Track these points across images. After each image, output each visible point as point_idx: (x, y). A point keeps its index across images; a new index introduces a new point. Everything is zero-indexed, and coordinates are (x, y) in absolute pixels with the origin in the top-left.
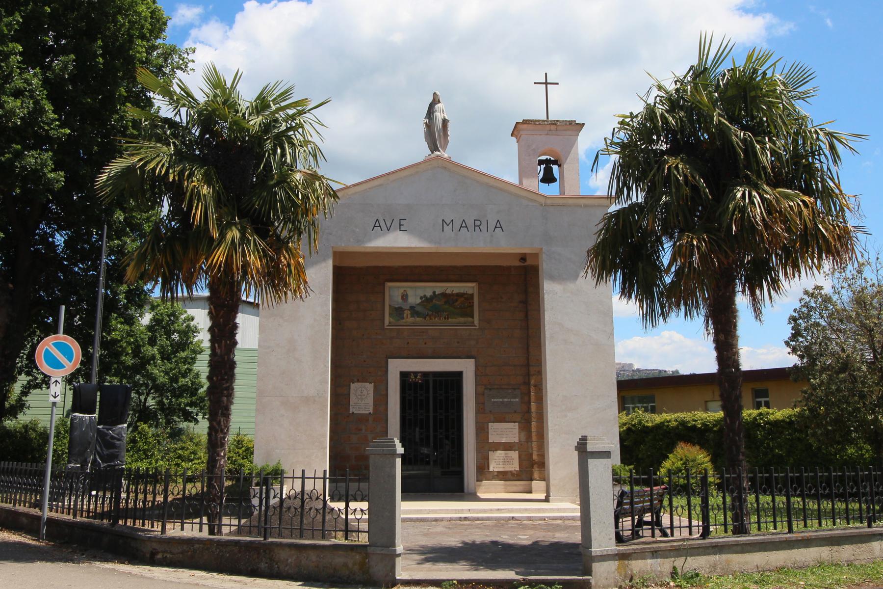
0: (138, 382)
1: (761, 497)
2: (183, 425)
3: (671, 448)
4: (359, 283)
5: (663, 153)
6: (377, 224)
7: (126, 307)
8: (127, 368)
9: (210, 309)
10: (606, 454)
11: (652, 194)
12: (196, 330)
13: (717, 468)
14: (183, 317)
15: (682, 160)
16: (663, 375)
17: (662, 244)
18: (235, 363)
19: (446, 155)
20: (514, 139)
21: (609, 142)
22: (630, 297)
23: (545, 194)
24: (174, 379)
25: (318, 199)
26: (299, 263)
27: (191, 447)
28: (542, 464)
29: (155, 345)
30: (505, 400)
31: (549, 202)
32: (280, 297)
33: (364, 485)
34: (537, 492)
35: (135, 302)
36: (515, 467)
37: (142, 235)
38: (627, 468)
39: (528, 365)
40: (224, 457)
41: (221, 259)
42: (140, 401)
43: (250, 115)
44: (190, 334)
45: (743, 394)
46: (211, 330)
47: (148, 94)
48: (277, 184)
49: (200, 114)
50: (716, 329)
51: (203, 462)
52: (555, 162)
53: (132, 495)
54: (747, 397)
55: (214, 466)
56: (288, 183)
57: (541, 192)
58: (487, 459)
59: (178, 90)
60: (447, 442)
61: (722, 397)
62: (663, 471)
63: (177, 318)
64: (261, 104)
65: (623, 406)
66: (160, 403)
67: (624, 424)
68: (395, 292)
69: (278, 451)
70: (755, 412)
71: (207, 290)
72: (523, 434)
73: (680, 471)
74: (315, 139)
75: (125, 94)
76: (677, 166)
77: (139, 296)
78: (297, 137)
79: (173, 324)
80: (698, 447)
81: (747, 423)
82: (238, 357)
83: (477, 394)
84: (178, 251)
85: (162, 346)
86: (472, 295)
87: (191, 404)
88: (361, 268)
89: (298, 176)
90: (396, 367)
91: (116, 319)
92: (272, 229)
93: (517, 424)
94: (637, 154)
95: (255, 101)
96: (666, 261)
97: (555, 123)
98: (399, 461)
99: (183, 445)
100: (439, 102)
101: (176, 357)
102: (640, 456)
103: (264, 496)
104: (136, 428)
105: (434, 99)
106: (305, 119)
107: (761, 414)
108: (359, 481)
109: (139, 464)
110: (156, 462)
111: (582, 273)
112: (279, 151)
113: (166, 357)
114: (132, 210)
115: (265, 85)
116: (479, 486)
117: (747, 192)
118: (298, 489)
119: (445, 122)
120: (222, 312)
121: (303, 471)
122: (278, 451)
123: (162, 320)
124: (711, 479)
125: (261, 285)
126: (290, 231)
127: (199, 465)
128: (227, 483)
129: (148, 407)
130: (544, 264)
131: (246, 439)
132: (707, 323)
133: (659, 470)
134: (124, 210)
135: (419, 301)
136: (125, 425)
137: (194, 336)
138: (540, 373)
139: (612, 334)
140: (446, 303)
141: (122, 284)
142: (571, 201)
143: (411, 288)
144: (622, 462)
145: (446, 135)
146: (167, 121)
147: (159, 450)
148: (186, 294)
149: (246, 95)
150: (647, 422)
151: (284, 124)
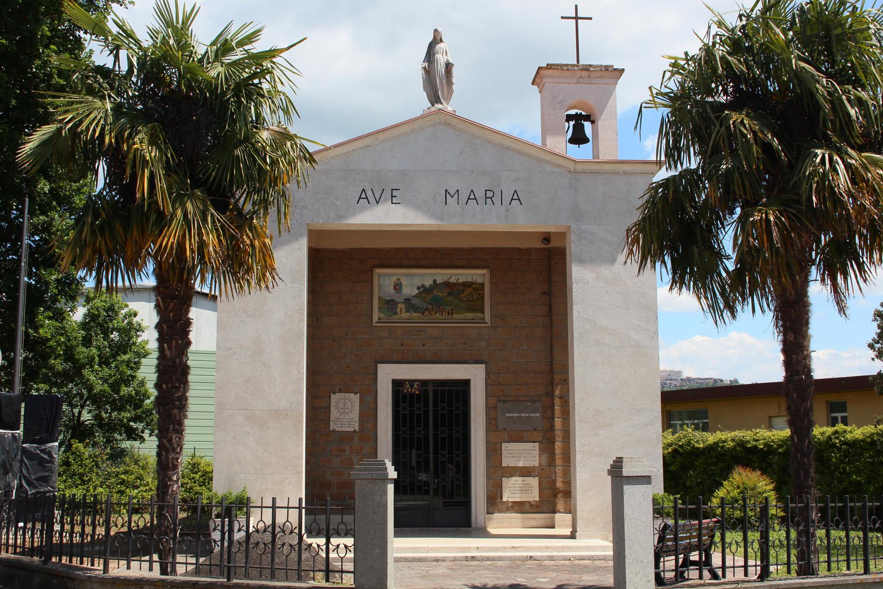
1: (833, 532)
2: (127, 444)
3: (726, 473)
4: (339, 268)
5: (722, 107)
6: (363, 196)
8: (57, 374)
10: (646, 480)
12: (139, 329)
14: (123, 312)
15: (747, 115)
16: (719, 384)
18: (188, 367)
19: (450, 109)
20: (535, 88)
26: (265, 244)
28: (568, 494)
30: (523, 415)
31: (579, 167)
32: (241, 287)
33: (348, 518)
34: (561, 526)
36: (534, 496)
37: (72, 210)
38: (672, 498)
39: (551, 372)
41: (171, 240)
42: (73, 415)
45: (814, 407)
46: (158, 326)
52: (588, 118)
53: (67, 527)
54: (819, 411)
55: (165, 493)
56: (253, 144)
59: (115, 29)
60: (450, 466)
61: (788, 408)
62: (715, 502)
63: (117, 314)
64: (223, 47)
65: (668, 422)
66: (98, 417)
67: (670, 445)
68: (386, 280)
69: (242, 476)
70: (829, 430)
72: (545, 456)
73: (737, 501)
75: (49, 34)
76: (742, 122)
79: (111, 321)
80: (759, 473)
81: (820, 443)
83: (488, 408)
84: (120, 230)
86: (483, 284)
87: (136, 419)
88: (343, 251)
89: (265, 135)
90: (388, 374)
97: (587, 68)
98: (391, 488)
100: (441, 41)
102: (688, 484)
103: (226, 528)
105: (435, 38)
110: (95, 490)
111: (622, 258)
116: (490, 519)
117: (827, 156)
119: (449, 66)
121: (274, 500)
122: (242, 476)
123: (99, 316)
124: (772, 511)
126: (254, 204)
127: (147, 490)
128: (182, 515)
131: (203, 462)
133: (710, 500)
135: (416, 292)
136: (56, 444)
137: (138, 336)
139: (656, 333)
140: (449, 294)
142: (607, 167)
143: (406, 275)
144: (666, 490)
145: (450, 83)
146: (102, 71)
147: (97, 473)
148: (127, 284)
149: (202, 37)
150: (697, 442)
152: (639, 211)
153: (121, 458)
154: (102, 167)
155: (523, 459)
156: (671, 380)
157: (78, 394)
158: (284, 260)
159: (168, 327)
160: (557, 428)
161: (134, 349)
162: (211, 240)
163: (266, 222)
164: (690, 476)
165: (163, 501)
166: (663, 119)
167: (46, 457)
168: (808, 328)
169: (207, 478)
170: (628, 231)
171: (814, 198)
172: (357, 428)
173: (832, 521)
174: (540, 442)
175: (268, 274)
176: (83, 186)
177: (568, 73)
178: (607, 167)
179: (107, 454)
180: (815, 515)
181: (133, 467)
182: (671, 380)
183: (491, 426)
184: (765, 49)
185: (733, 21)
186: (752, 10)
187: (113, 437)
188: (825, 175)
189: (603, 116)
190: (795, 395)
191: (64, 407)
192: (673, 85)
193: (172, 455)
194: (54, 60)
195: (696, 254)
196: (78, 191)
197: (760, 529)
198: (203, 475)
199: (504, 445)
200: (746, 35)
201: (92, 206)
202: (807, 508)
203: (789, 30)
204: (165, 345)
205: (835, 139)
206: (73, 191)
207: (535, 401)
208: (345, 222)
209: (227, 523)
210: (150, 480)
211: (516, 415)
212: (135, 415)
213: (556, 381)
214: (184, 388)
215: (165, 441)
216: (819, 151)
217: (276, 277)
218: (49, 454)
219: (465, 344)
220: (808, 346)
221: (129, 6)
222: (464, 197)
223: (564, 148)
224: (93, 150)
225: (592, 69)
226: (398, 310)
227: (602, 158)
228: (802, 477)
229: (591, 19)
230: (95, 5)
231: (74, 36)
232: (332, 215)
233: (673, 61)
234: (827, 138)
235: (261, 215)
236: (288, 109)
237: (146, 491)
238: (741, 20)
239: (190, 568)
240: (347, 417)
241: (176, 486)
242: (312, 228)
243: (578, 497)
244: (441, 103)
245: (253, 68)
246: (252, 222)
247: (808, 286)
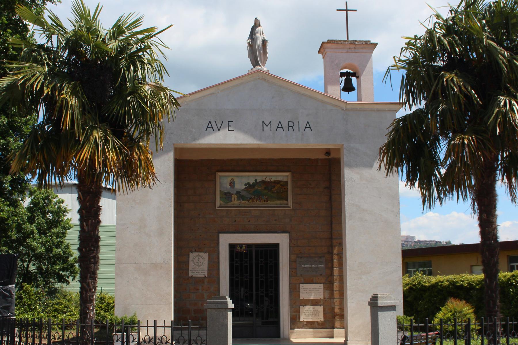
0: (21, 252)
1: (511, 339)
2: (58, 285)
3: (443, 302)
4: (195, 172)
5: (440, 69)
6: (210, 126)
7: (11, 193)
8: (13, 241)
9: (79, 195)
10: (392, 308)
11: (432, 102)
12: (66, 211)
13: (477, 319)
14: (55, 200)
15: (456, 74)
16: (439, 245)
17: (438, 140)
18: (99, 237)
19: (265, 69)
20: (320, 56)
21: (397, 59)
22: (412, 184)
23: (346, 100)
24: (49, 250)
25: (163, 106)
26: (147, 158)
27: (65, 302)
28: (342, 316)
29: (34, 223)
30: (313, 266)
31: (349, 107)
32: (132, 186)
33: (203, 332)
34: (337, 337)
35: (18, 188)
36: (320, 318)
37: (22, 136)
38: (408, 318)
39: (331, 238)
40: (93, 310)
41: (86, 156)
42: (24, 267)
43: (108, 40)
44: (61, 214)
45: (500, 261)
46: (80, 211)
47: (24, 22)
48: (130, 94)
49: (68, 40)
50: (480, 209)
51: (74, 314)
52: (354, 75)
53: (24, 339)
54: (503, 262)
55: (85, 318)
56: (139, 94)
57: (343, 99)
58: (298, 312)
59: (50, 22)
60: (266, 299)
61: (484, 263)
62: (436, 321)
63: (50, 201)
64: (118, 30)
65: (406, 269)
66: (39, 268)
67: (407, 284)
68: (224, 180)
69: (133, 306)
70: (509, 274)
71: (76, 180)
72: (327, 292)
73: (450, 320)
74: (161, 59)
75: (6, 22)
76: (452, 79)
77: (21, 184)
78: (146, 57)
79: (47, 206)
80: (464, 302)
81: (503, 282)
82: (102, 232)
83: (291, 261)
84: (53, 149)
85: (39, 224)
86: (287, 182)
87: (64, 270)
88: (197, 161)
89: (147, 88)
90: (226, 240)
91: (4, 202)
92: (126, 131)
93: (322, 285)
94: (422, 69)
95: (112, 28)
96: (442, 156)
97: (353, 43)
98: (230, 314)
99: (59, 301)
100: (259, 25)
101: (50, 232)
102: (419, 309)
103: (125, 340)
104: (21, 288)
105: (255, 24)
106: (152, 42)
107: (513, 276)
108: (199, 329)
109: (25, 315)
110: (38, 314)
111: (376, 165)
112: (132, 68)
113: (42, 232)
114: (14, 115)
115: (120, 16)
116: (293, 332)
117: (508, 101)
118: (151, 333)
119: (264, 42)
120: (88, 197)
121: (155, 322)
122: (133, 306)
123: (39, 203)
124: (472, 326)
125: (117, 177)
126: (140, 133)
127: (74, 314)
128: (96, 330)
129: (30, 271)
130: (345, 157)
131: (107, 296)
132: (474, 204)
133: (433, 320)
134: (7, 115)
135: (244, 187)
136: (14, 285)
137: (64, 216)
138: (341, 244)
139: (398, 213)
140: (265, 188)
141: (7, 174)
142: (366, 107)
143: (237, 176)
144: (405, 313)
145: (265, 52)
146: (41, 46)
147: (40, 304)
148: (58, 182)
149: (105, 25)
150: (425, 282)
151: (135, 46)
152: (387, 137)
153: (55, 294)
154: (42, 109)
155: (313, 294)
156: (408, 242)
157: (26, 253)
158: (159, 167)
159: (86, 212)
160: (335, 274)
161: (62, 224)
162: (111, 155)
163: (148, 143)
164: (420, 304)
165: (84, 323)
166: (403, 76)
167: (7, 294)
168: (495, 210)
169: (110, 307)
170: (381, 149)
171: (498, 129)
172: (206, 275)
173: (510, 333)
174: (324, 283)
175: (150, 177)
176: (29, 120)
177: (341, 46)
178: (366, 107)
179: (46, 291)
180: (499, 330)
181: (63, 300)
182: (408, 242)
183: (293, 273)
184: (467, 32)
185: (446, 15)
186: (459, 6)
187: (49, 281)
188: (506, 113)
189: (364, 73)
190: (487, 253)
191: (18, 262)
192: (408, 55)
193: (90, 294)
194: (10, 39)
195: (422, 162)
196: (26, 123)
197: (465, 339)
198: (107, 306)
199: (301, 285)
200: (454, 23)
201: (36, 134)
202: (494, 325)
203: (483, 19)
204: (84, 223)
205: (512, 90)
206: (23, 123)
207: (320, 257)
208: (198, 142)
209: (125, 337)
210: (73, 308)
211: (309, 266)
212: (63, 267)
213: (334, 245)
214: (97, 251)
215: (85, 285)
216: (502, 98)
217: (155, 179)
218: (10, 292)
219: (276, 220)
220: (496, 222)
221: (57, 3)
222: (274, 126)
223: (339, 94)
224: (37, 97)
225: (356, 43)
226: (233, 199)
227: (364, 100)
228: (492, 305)
229: (356, 11)
230: (36, 3)
231: (23, 23)
232: (189, 138)
233: (407, 41)
234: (507, 89)
235: (145, 139)
236: (161, 70)
237: (71, 315)
238: (452, 14)
239: (37, 334)
240: (200, 268)
241: (92, 313)
242: (176, 146)
243: (349, 318)
244: (260, 66)
245: (139, 44)
246: (139, 145)
247: (495, 184)
